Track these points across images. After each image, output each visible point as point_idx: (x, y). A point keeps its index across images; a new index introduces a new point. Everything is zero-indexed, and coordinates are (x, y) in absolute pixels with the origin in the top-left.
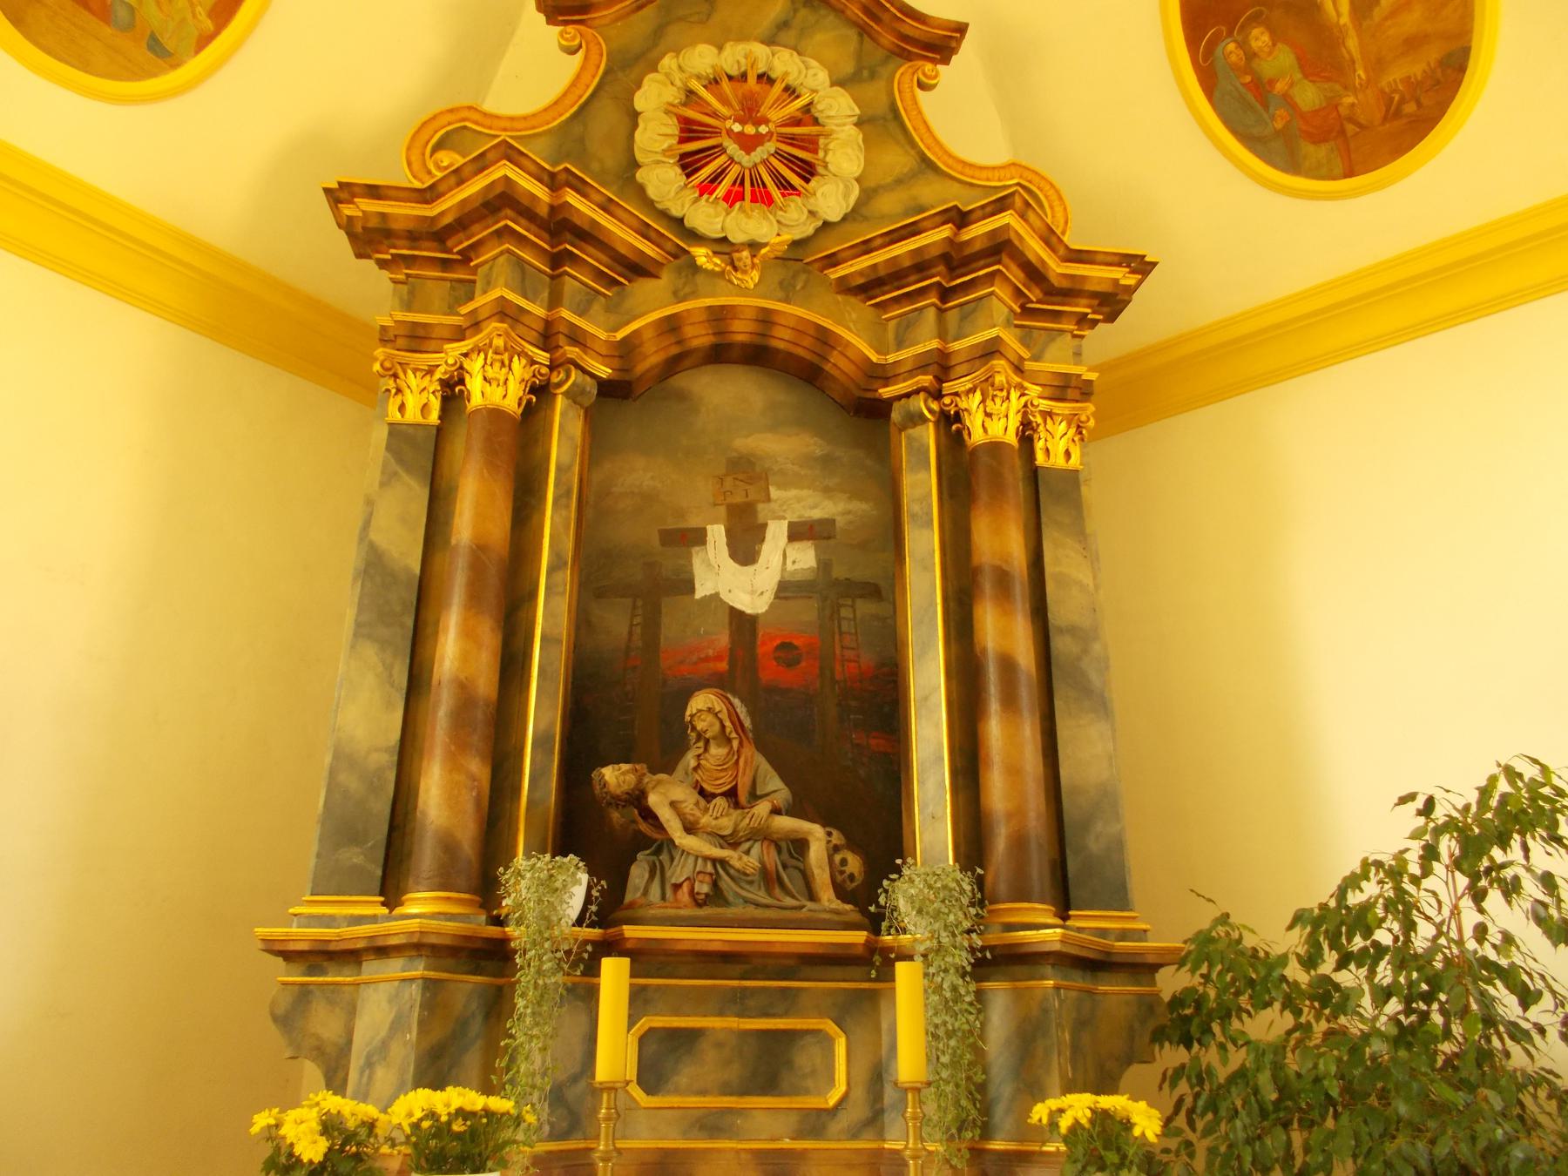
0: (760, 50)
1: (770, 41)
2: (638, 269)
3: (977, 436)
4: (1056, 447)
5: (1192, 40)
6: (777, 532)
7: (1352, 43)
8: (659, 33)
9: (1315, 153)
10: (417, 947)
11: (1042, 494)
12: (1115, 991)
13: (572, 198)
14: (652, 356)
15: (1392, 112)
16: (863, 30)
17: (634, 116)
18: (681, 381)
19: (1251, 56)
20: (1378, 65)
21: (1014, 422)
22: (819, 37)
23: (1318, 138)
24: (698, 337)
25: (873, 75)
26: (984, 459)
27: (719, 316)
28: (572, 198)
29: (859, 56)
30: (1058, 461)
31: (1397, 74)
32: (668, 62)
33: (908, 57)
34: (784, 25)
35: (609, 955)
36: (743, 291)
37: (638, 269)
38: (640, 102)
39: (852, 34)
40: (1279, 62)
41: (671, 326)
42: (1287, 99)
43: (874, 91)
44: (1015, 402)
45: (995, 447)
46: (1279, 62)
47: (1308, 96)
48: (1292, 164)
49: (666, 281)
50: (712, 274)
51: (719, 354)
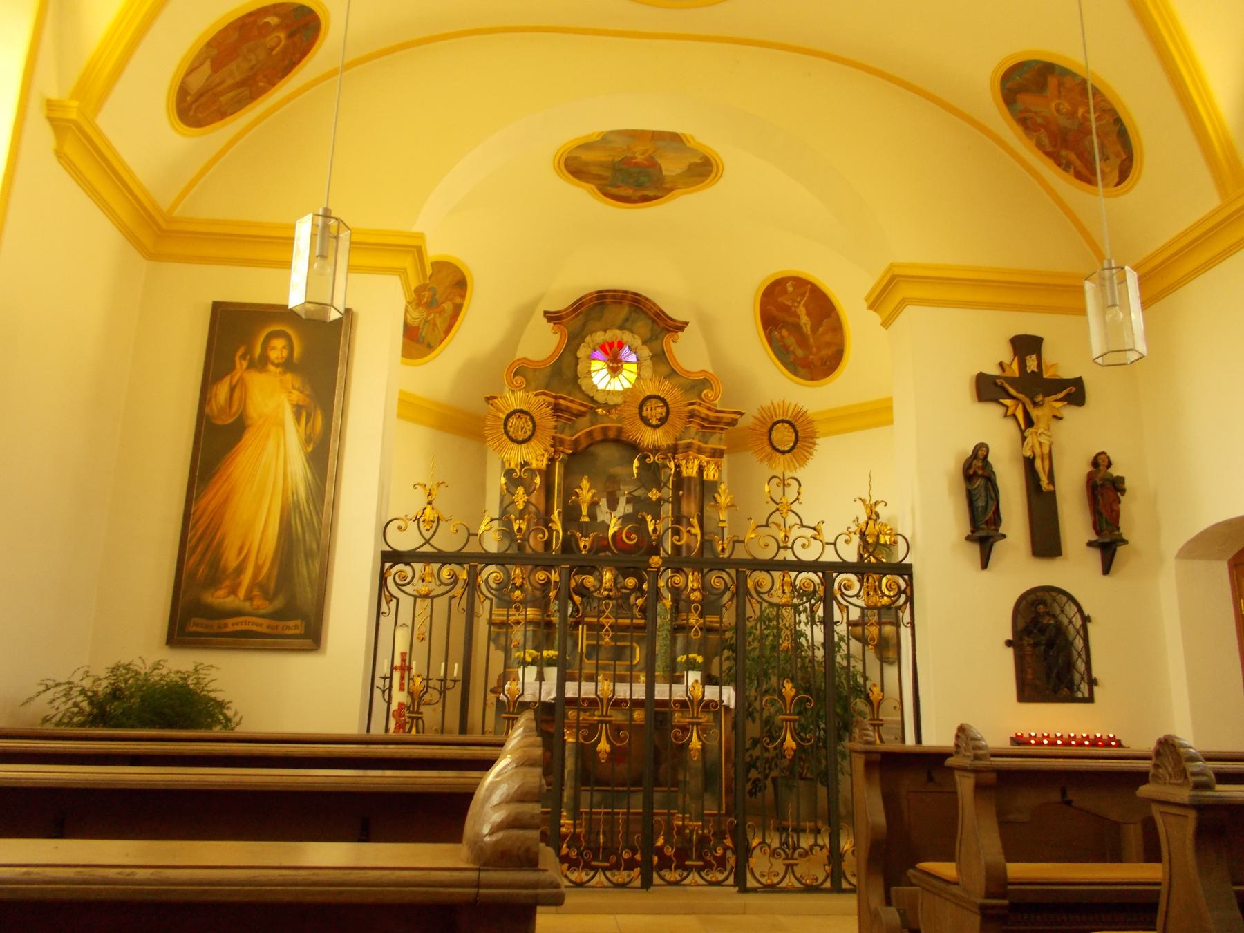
0: (618, 332)
1: (621, 328)
2: (580, 415)
3: (684, 474)
4: (710, 473)
5: (765, 329)
6: (623, 500)
7: (811, 340)
8: (584, 325)
9: (803, 371)
10: (531, 622)
11: (706, 489)
12: (713, 637)
13: (561, 401)
14: (584, 444)
15: (824, 364)
16: (654, 321)
17: (577, 359)
18: (592, 449)
19: (783, 337)
20: (819, 349)
21: (696, 469)
22: (639, 324)
23: (803, 367)
24: (598, 436)
25: (657, 338)
26: (686, 482)
27: (605, 430)
28: (561, 401)
29: (652, 331)
30: (711, 478)
31: (824, 353)
32: (588, 339)
33: (669, 331)
34: (627, 320)
35: (736, 690)
36: (612, 421)
37: (580, 415)
38: (579, 354)
39: (649, 322)
40: (791, 341)
41: (590, 434)
42: (794, 353)
43: (656, 344)
44: (697, 462)
45: (690, 478)
46: (791, 341)
47: (800, 353)
48: (795, 373)
49: (588, 417)
50: (603, 415)
51: (605, 440)
